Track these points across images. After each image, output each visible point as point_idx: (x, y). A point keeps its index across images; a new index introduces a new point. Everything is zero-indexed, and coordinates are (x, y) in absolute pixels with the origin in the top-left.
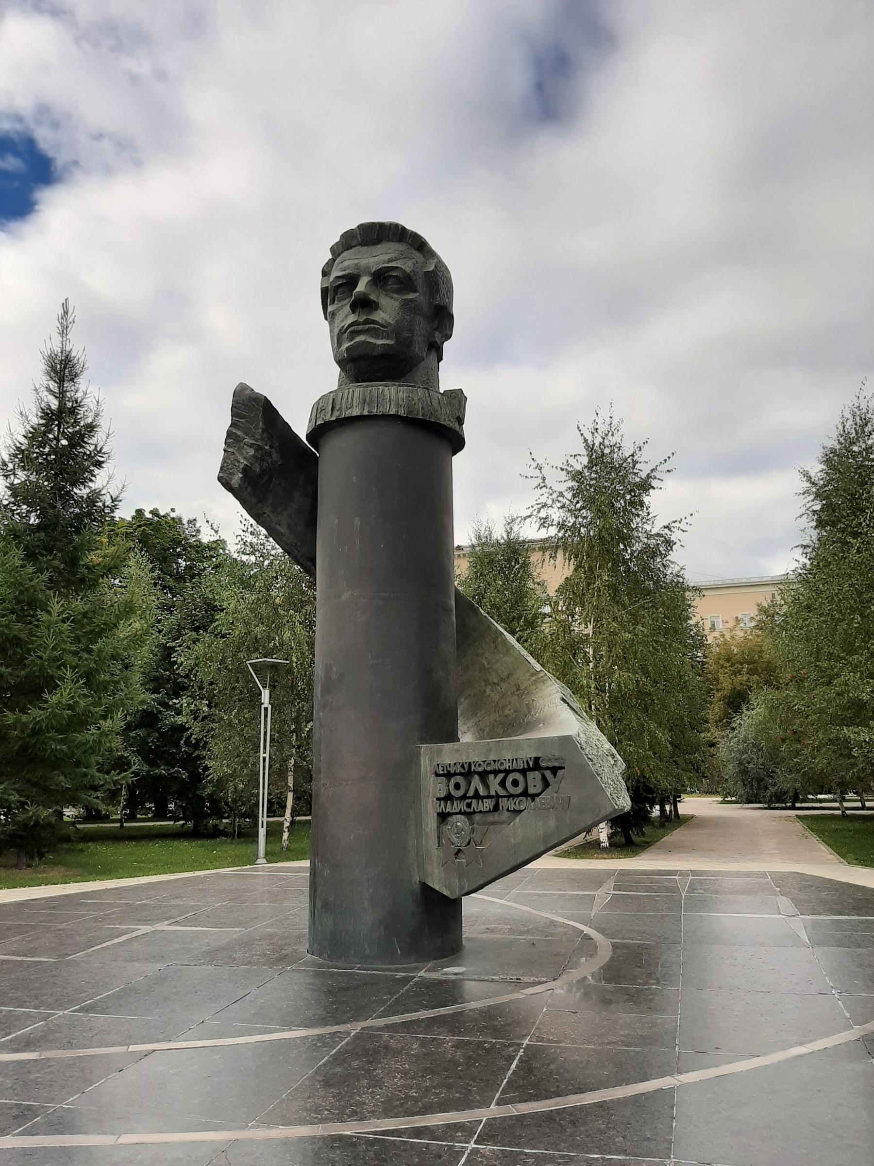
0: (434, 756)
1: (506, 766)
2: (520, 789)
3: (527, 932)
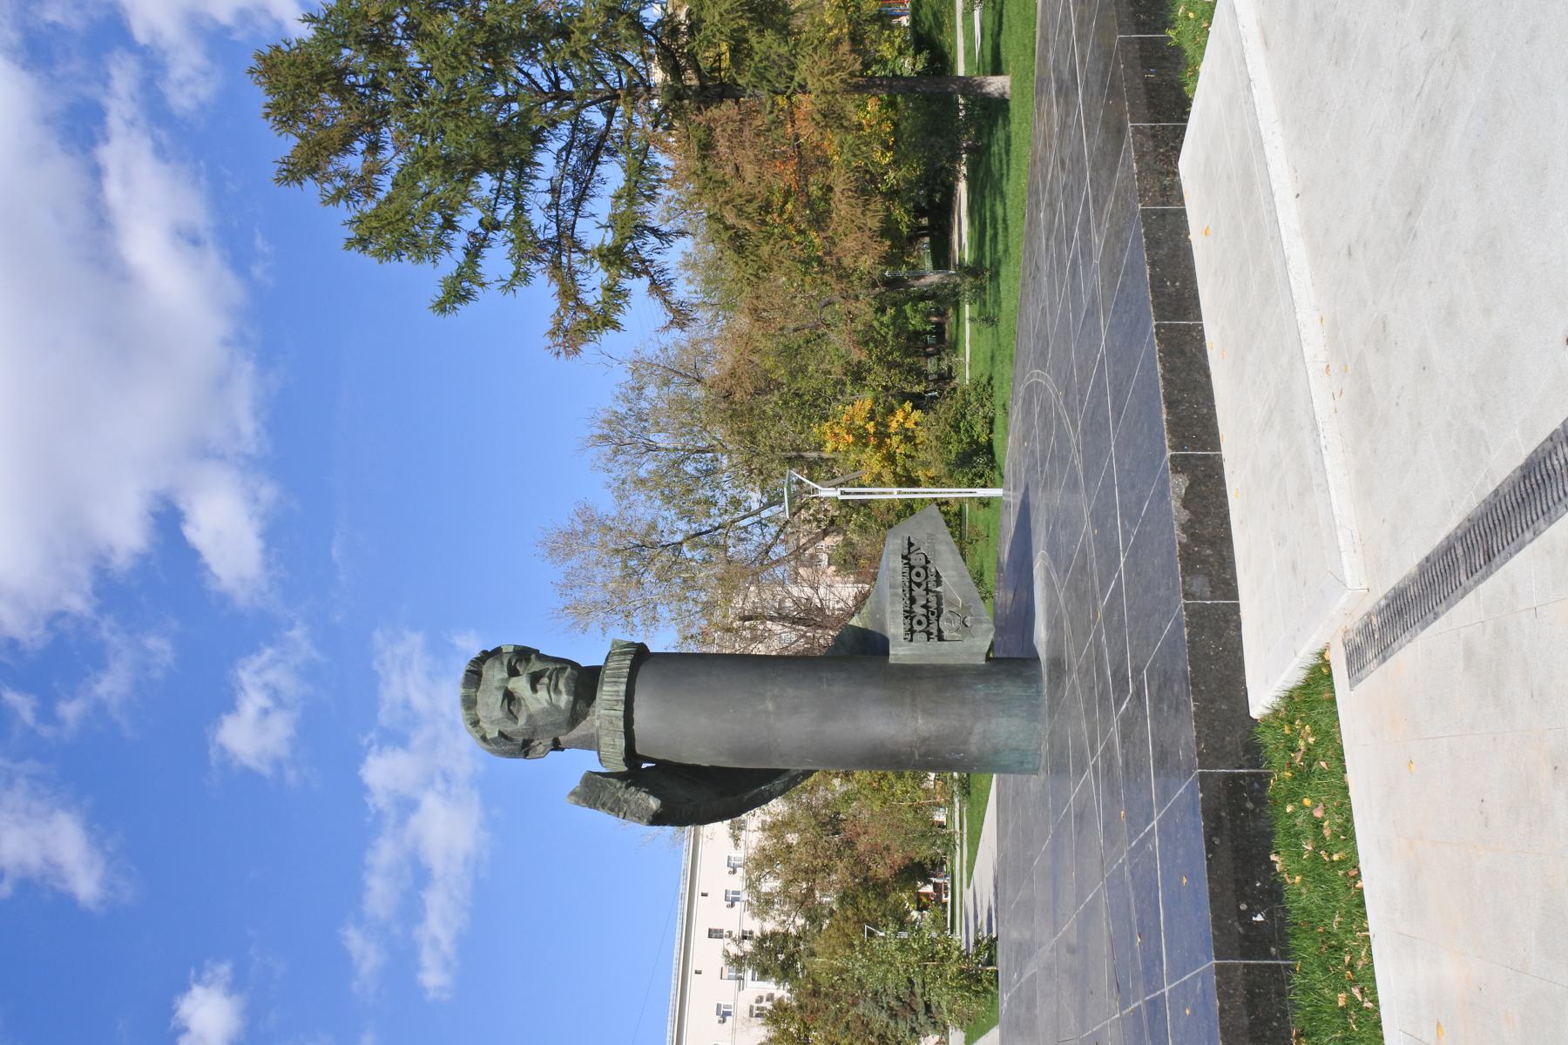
0: (901, 652)
1: (906, 580)
2: (922, 572)
3: (1148, 930)
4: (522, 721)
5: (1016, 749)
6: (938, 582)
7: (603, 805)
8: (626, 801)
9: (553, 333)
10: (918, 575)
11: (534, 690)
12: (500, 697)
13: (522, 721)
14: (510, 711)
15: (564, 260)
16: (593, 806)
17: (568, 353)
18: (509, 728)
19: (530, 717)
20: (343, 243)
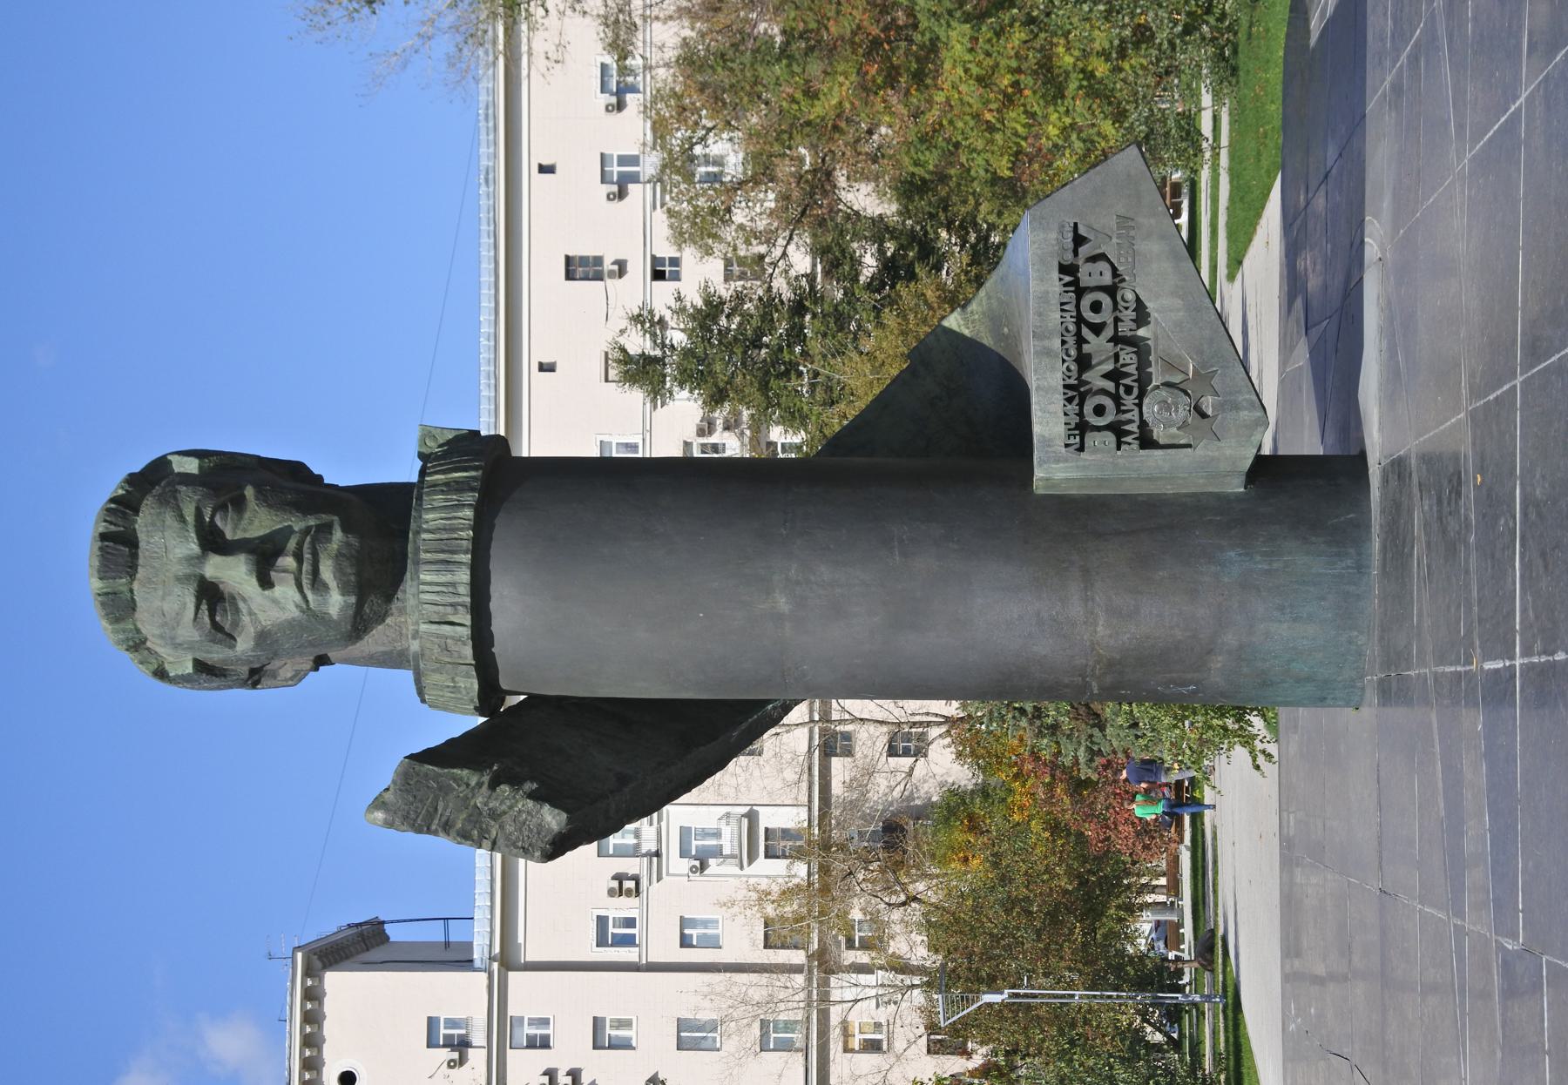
0: (1055, 466)
5: (1309, 679)
6: (1142, 316)
7: (446, 827)
8: (495, 815)
11: (266, 583)
12: (190, 602)
14: (216, 627)
16: (424, 828)
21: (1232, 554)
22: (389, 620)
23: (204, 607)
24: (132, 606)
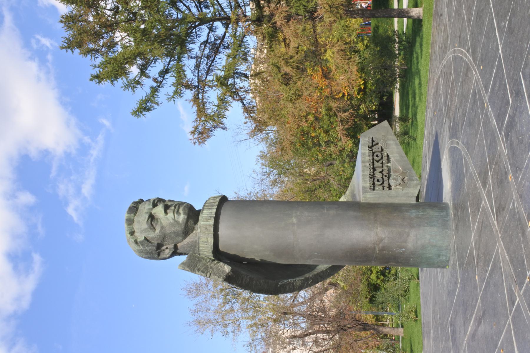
1: (371, 158)
2: (379, 154)
4: (158, 230)
5: (434, 246)
6: (389, 161)
7: (199, 270)
8: (211, 268)
9: (193, 133)
10: (377, 156)
11: (166, 213)
12: (147, 217)
13: (158, 230)
15: (200, 96)
17: (200, 143)
18: (151, 235)
19: (162, 227)
20: (90, 77)
21: (413, 211)
22: (194, 232)
23: (150, 219)
24: (133, 221)
